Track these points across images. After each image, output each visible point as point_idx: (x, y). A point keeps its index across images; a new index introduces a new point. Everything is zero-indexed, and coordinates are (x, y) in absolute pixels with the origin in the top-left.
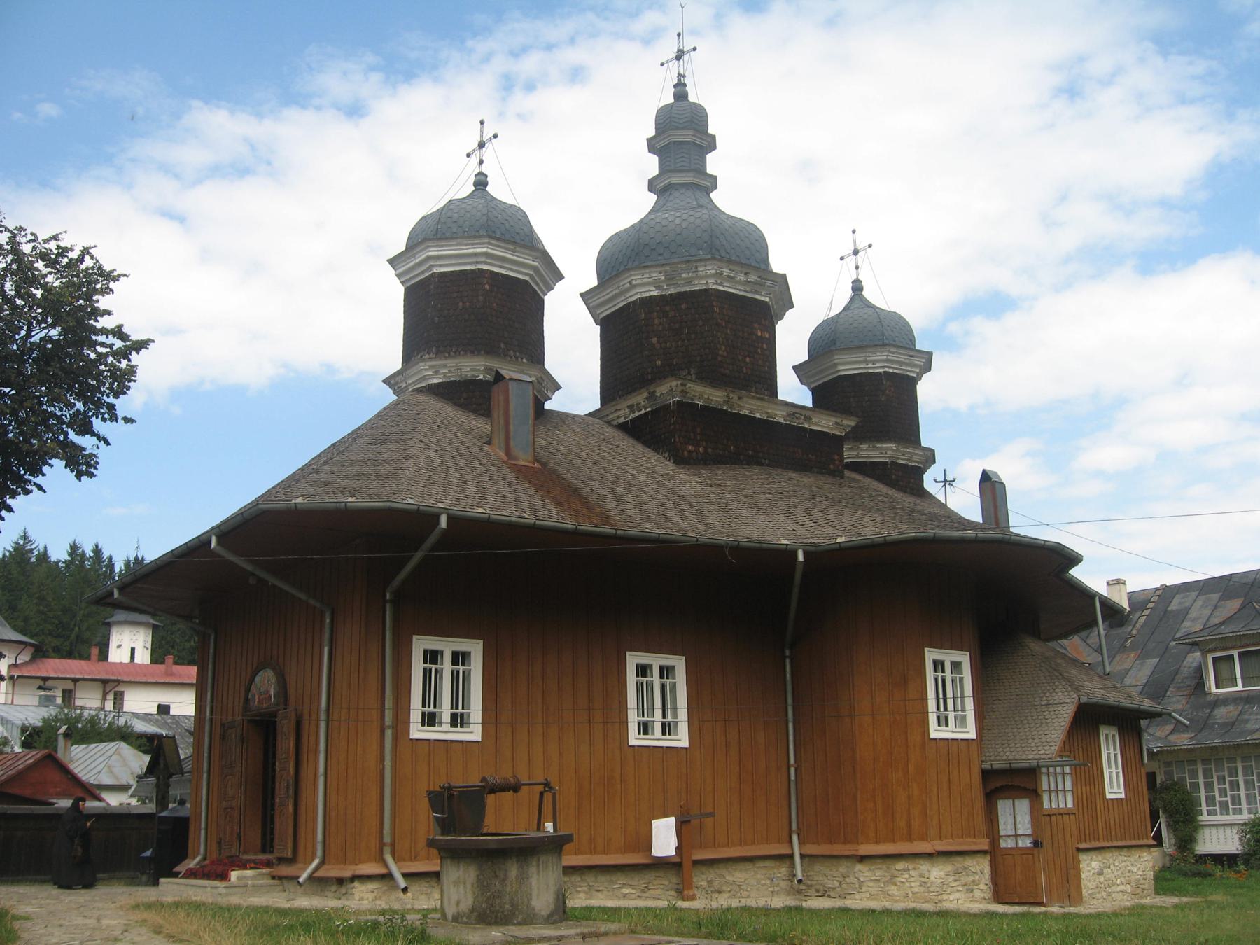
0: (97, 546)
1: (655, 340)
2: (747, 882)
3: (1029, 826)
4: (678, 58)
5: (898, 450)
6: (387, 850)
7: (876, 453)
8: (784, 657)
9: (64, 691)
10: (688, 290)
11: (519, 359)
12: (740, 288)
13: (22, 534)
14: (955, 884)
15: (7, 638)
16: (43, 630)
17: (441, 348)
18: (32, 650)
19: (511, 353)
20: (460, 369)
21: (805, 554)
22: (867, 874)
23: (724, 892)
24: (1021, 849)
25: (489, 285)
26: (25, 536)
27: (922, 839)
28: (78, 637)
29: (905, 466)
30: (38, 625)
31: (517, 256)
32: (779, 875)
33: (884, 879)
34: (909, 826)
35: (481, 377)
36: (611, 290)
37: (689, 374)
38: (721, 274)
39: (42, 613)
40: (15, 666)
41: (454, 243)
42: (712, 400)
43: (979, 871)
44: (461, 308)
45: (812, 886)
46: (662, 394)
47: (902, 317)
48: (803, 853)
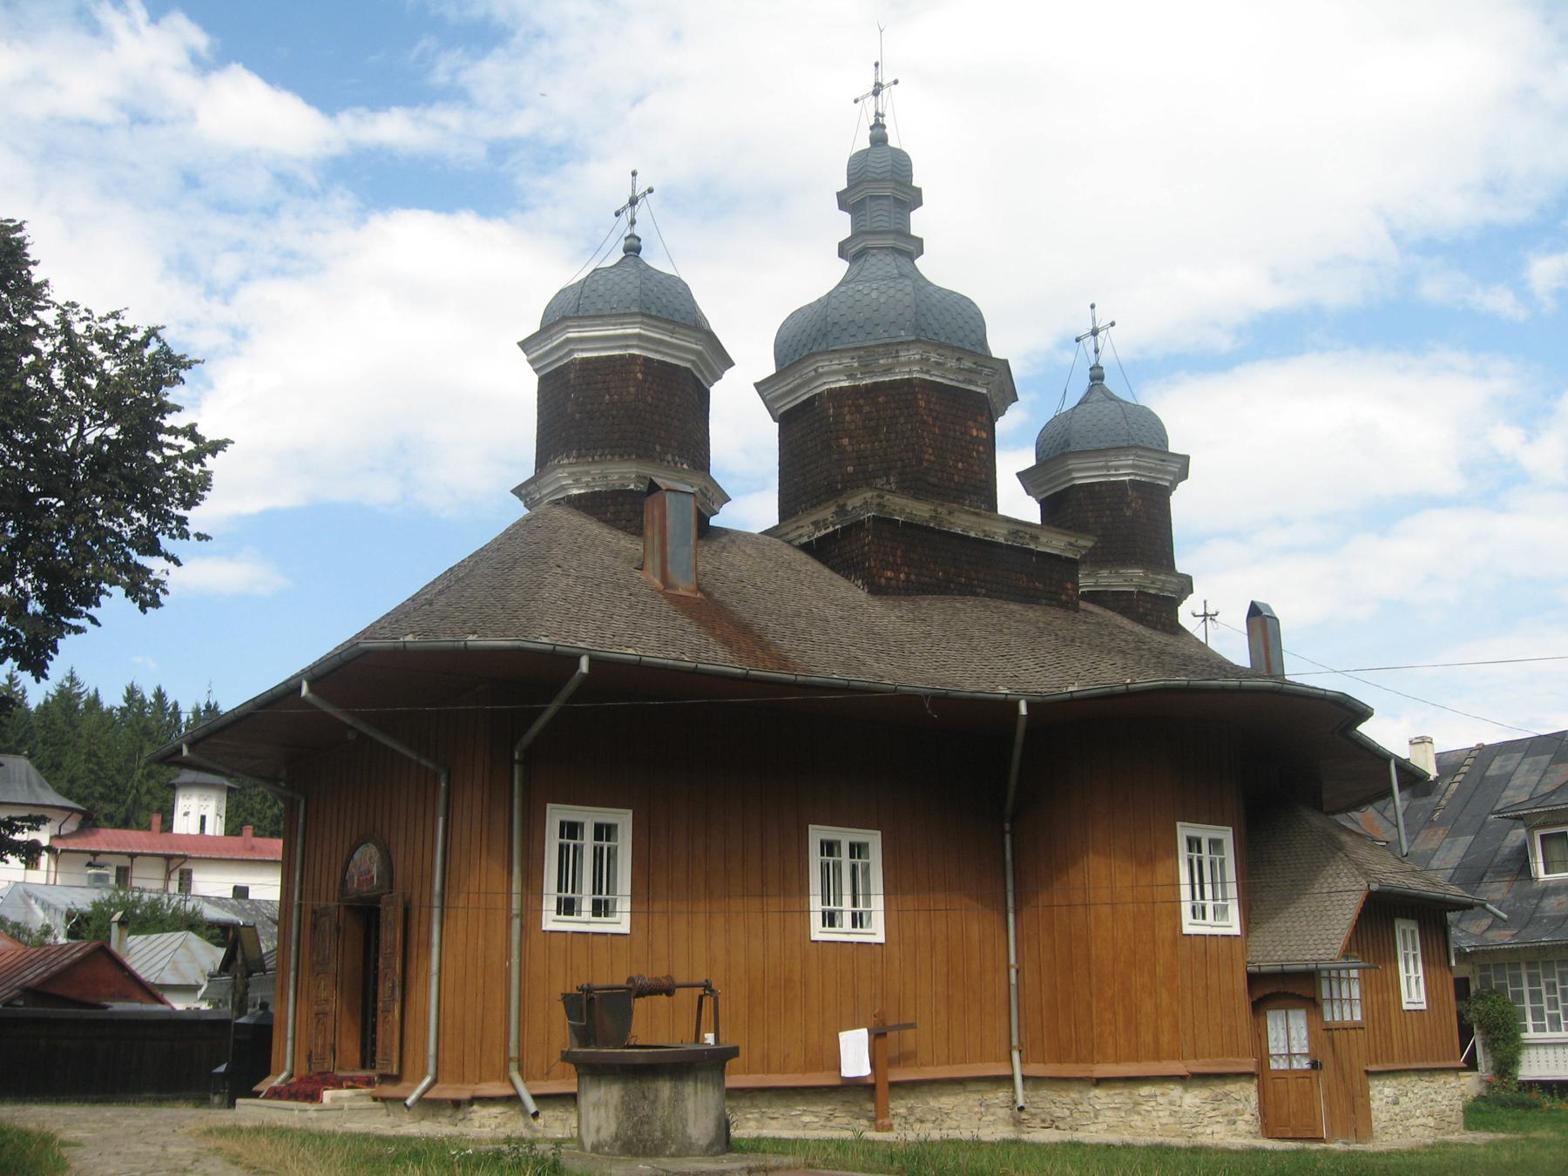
0: (159, 689)
1: (846, 441)
2: (955, 1109)
3: (1306, 1042)
4: (876, 93)
6: (513, 1067)
7: (1120, 581)
8: (1003, 833)
11: (679, 465)
12: (951, 377)
16: (93, 793)
18: (80, 817)
19: (669, 457)
24: (1296, 1071)
25: (642, 373)
27: (1173, 1058)
28: (135, 801)
29: (1156, 596)
30: (87, 787)
31: (677, 339)
32: (996, 1101)
33: (1125, 1107)
35: (632, 487)
38: (928, 360)
39: (91, 771)
41: (599, 322)
42: (916, 515)
43: (1243, 1099)
45: (1036, 1114)
46: (854, 508)
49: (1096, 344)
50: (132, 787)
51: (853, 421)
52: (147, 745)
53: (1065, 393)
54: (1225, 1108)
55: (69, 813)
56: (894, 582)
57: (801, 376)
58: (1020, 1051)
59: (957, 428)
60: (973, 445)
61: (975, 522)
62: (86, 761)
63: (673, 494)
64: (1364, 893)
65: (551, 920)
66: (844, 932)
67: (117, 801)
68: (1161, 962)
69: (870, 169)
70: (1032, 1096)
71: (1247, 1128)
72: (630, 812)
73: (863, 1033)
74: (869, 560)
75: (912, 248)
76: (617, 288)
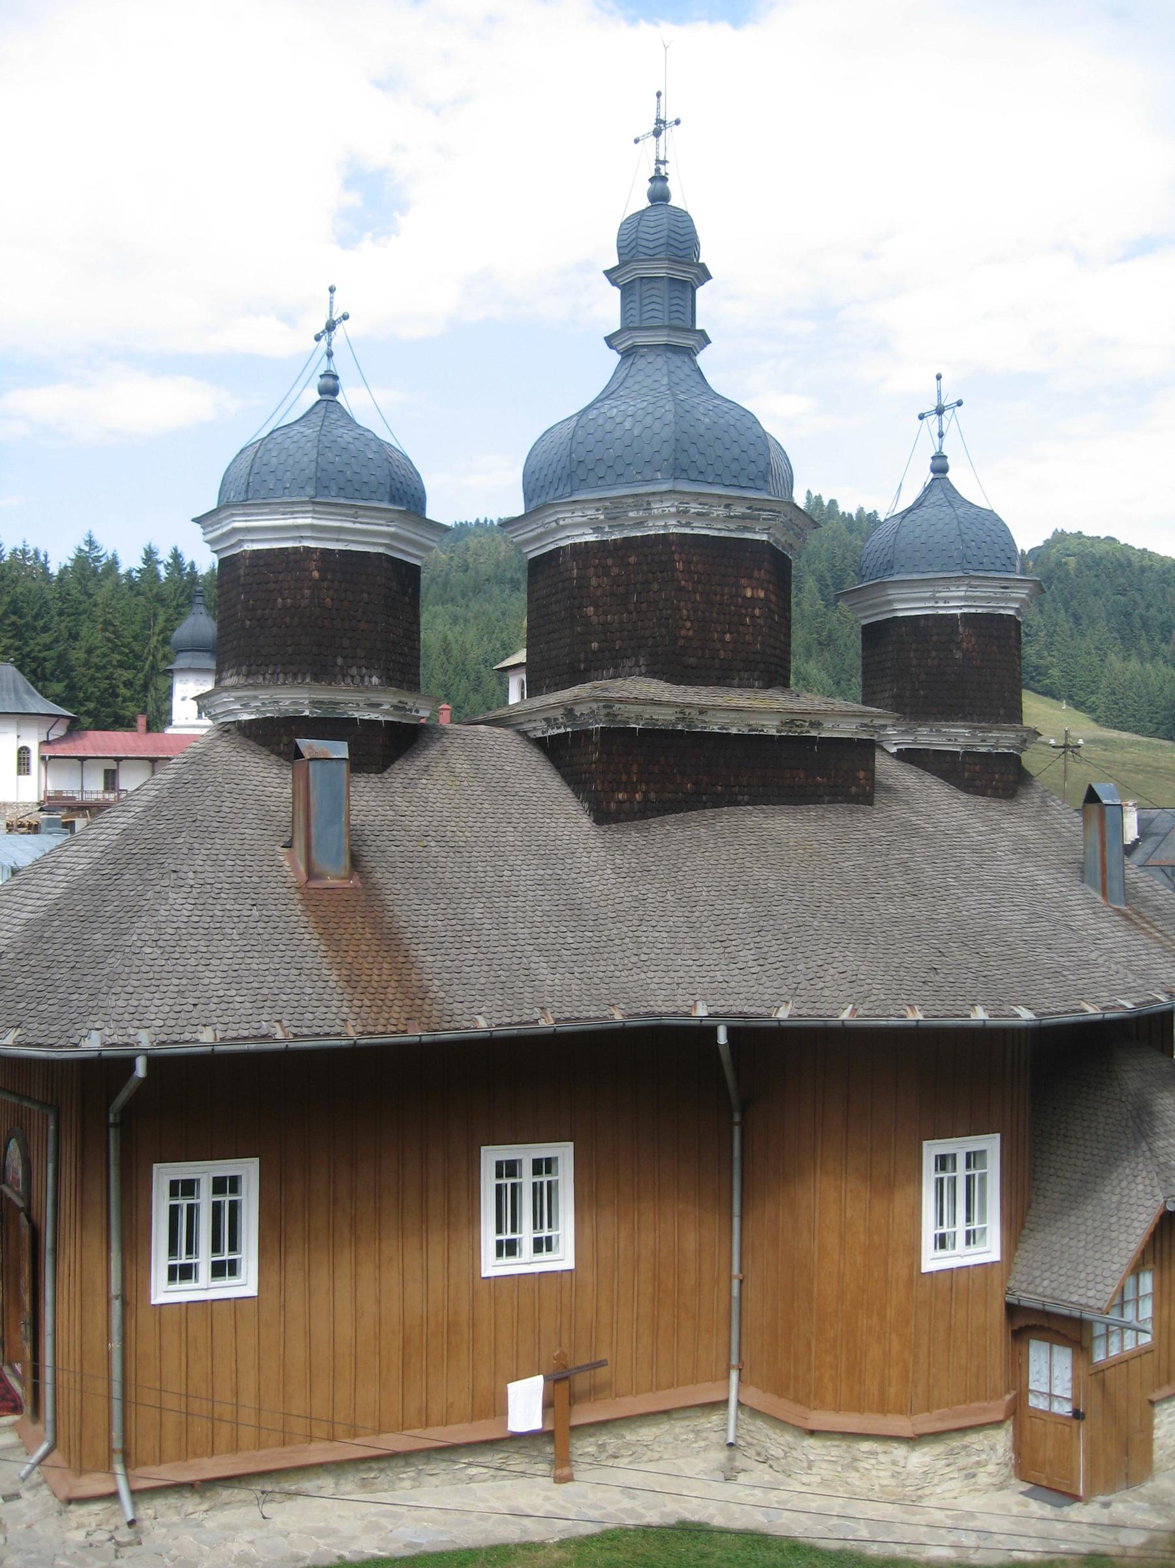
0: (176, 550)
1: (590, 610)
2: (657, 1439)
3: (1069, 1385)
4: (657, 133)
5: (974, 736)
6: (117, 1458)
7: (943, 740)
8: (731, 1124)
9: (106, 772)
10: (639, 534)
11: (367, 679)
12: (719, 527)
13: (88, 539)
14: (948, 1469)
15: (35, 711)
16: (111, 661)
17: (254, 667)
18: (67, 722)
19: (354, 671)
20: (277, 702)
21: (731, 1031)
23: (622, 1456)
25: (318, 571)
26: (90, 540)
27: (900, 1411)
28: (153, 667)
29: (988, 754)
31: (361, 523)
32: (709, 1425)
33: (842, 1461)
34: (882, 1392)
35: (307, 713)
38: (686, 512)
39: (108, 640)
40: (47, 743)
41: (266, 510)
42: (657, 720)
43: (987, 1448)
45: (752, 1444)
46: (582, 714)
47: (999, 520)
48: (742, 1400)
49: (941, 426)
50: (149, 653)
51: (599, 585)
52: (161, 610)
53: (899, 489)
54: (963, 1461)
55: (56, 719)
56: (627, 805)
57: (543, 525)
58: (740, 1370)
59: (726, 589)
61: (735, 718)
63: (318, 764)
64: (1158, 1211)
66: (527, 1262)
67: (135, 668)
69: (641, 249)
70: (749, 1424)
71: (990, 1481)
74: (596, 782)
75: (692, 343)
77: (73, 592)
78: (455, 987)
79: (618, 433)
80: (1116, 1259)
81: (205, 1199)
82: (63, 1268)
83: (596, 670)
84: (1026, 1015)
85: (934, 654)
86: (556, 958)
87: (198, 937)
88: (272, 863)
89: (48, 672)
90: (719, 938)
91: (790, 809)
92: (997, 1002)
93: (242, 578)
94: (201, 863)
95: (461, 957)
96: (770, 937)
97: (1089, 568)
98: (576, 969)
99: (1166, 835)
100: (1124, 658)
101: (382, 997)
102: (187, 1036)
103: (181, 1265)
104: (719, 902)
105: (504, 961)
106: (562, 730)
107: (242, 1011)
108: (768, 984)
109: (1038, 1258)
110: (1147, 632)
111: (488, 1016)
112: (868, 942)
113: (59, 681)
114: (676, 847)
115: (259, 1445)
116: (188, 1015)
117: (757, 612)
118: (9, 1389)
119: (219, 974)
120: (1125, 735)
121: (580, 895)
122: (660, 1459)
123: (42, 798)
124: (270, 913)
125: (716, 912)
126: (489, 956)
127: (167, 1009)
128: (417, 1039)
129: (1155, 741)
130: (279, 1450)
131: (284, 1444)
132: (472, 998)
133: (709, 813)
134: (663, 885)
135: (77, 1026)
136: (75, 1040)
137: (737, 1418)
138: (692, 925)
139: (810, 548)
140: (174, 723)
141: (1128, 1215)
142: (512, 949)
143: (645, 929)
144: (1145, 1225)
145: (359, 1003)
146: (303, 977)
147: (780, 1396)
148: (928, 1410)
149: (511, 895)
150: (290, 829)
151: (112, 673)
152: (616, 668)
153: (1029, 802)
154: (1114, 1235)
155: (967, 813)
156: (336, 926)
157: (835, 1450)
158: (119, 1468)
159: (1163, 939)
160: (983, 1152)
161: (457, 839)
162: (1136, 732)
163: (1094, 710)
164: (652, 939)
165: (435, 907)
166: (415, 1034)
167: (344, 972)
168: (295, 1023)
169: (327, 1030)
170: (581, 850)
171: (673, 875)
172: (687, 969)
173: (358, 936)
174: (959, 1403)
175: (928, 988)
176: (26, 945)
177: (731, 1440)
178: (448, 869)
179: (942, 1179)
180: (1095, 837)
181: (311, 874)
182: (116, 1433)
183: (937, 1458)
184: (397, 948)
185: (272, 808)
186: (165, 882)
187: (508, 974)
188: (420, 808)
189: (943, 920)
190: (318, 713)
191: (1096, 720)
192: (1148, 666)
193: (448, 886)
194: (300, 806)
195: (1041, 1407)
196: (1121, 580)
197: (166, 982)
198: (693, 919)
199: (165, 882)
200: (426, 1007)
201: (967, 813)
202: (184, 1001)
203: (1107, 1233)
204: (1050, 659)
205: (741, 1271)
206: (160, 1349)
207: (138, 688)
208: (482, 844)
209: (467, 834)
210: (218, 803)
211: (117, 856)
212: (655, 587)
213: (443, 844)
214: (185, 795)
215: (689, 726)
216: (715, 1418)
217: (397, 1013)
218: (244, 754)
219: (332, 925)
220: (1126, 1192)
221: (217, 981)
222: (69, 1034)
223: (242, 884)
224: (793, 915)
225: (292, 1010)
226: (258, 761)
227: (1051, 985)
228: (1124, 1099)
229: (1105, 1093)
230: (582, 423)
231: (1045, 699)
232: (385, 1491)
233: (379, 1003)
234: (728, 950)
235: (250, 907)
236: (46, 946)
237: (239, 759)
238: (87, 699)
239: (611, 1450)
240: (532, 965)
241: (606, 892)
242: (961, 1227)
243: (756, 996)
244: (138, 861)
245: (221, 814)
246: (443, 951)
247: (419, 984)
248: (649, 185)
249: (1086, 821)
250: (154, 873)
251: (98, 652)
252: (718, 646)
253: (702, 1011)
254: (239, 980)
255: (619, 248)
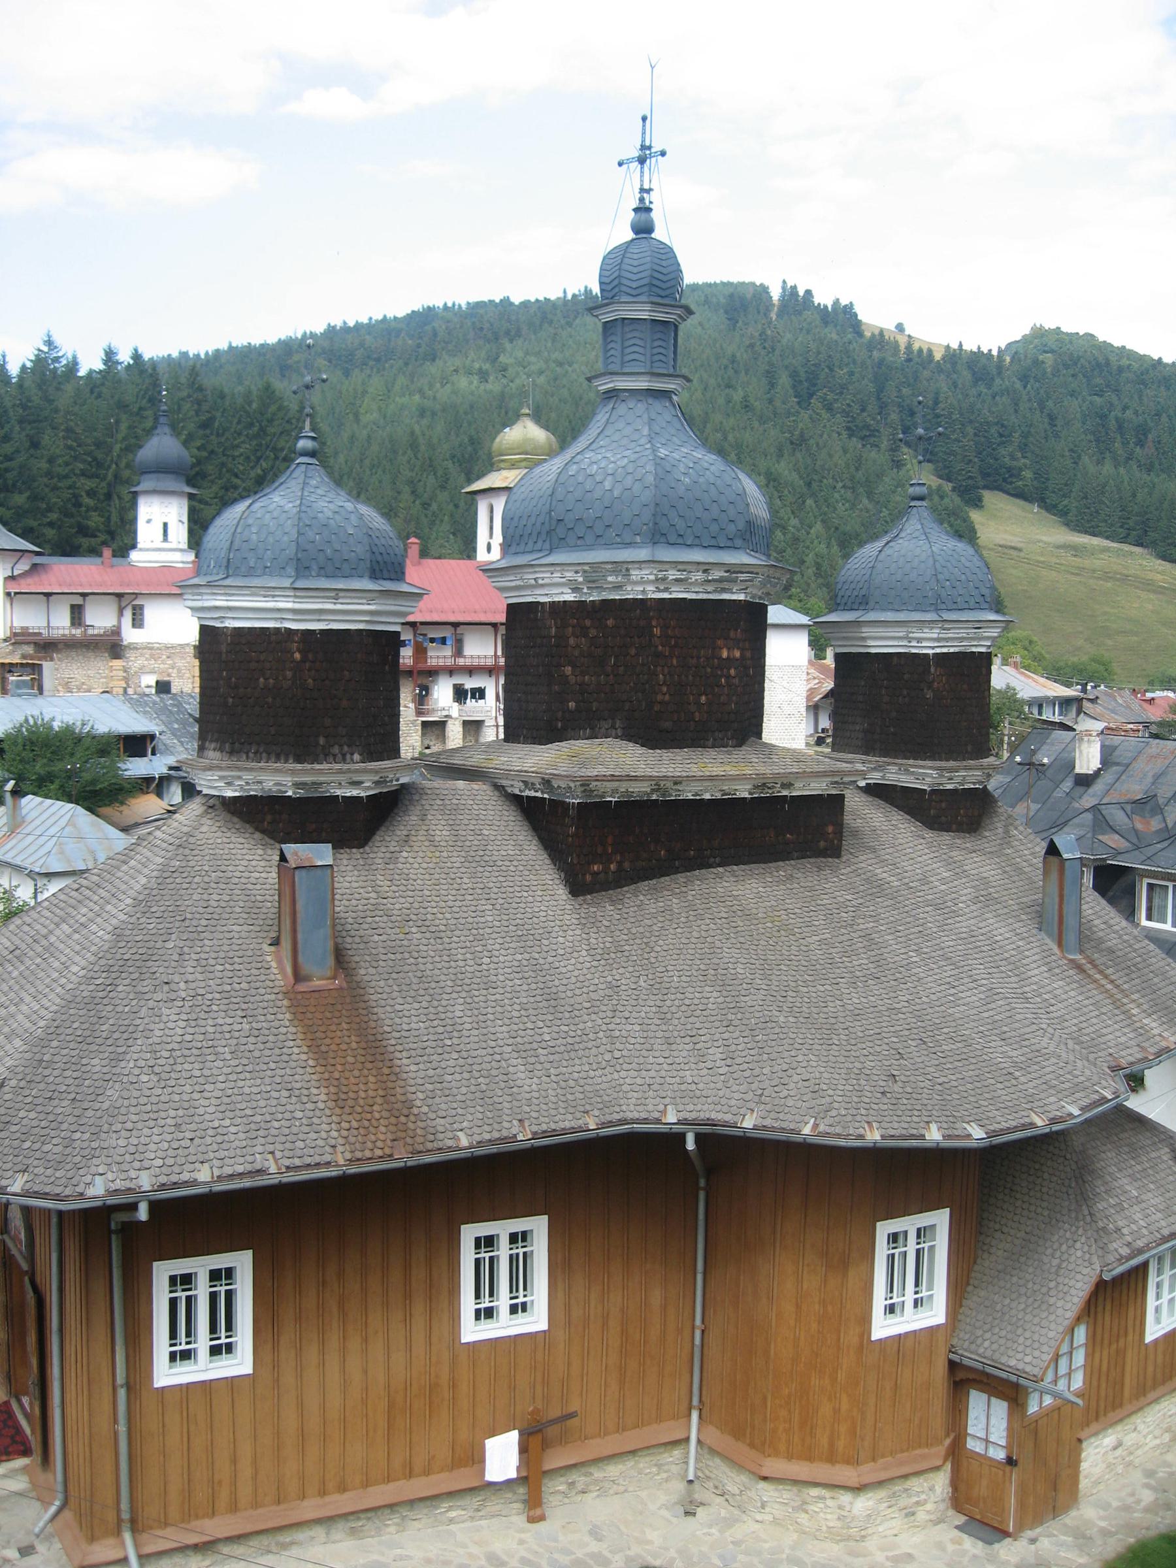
0: (136, 350)
3: (1005, 1434)
6: (126, 1527)
7: (911, 778)
8: (697, 1189)
9: (73, 607)
11: (348, 756)
14: (890, 1510)
17: (237, 745)
21: (699, 1137)
22: (772, 1493)
24: (991, 1459)
28: (116, 476)
29: (955, 791)
30: (67, 464)
34: (832, 1444)
35: (290, 793)
36: (512, 578)
37: (613, 727)
39: (70, 448)
40: (12, 578)
43: (926, 1489)
44: (261, 686)
50: (112, 461)
52: (124, 417)
54: (904, 1501)
56: (602, 876)
57: (521, 579)
60: (722, 670)
62: (64, 438)
63: (304, 872)
65: (165, 1375)
66: (505, 1326)
67: (97, 476)
68: (844, 1367)
69: (624, 288)
71: (928, 1517)
72: (250, 1253)
73: (513, 1436)
76: (271, 540)
77: (35, 398)
78: (437, 1100)
79: (598, 494)
80: (1053, 1326)
81: (202, 1291)
82: (70, 1350)
83: (573, 729)
84: (977, 1133)
85: (905, 692)
86: (533, 1060)
87: (192, 1059)
88: (259, 965)
89: (10, 482)
90: (689, 1033)
91: (757, 868)
92: (951, 1119)
93: (224, 656)
94: (192, 970)
95: (443, 1064)
96: (737, 1034)
97: (1066, 366)
98: (552, 1071)
99: (1128, 766)
100: (1098, 462)
101: (369, 1116)
102: (185, 1176)
103: (181, 1351)
104: (690, 989)
105: (484, 1066)
106: (539, 794)
107: (237, 1142)
108: (735, 1088)
109: (981, 1317)
110: (1122, 435)
111: (469, 1132)
112: (830, 1042)
113: (20, 493)
114: (649, 922)
115: (256, 1505)
116: (186, 1152)
117: (732, 672)
118: (18, 1429)
119: (213, 1101)
120: (1096, 541)
121: (557, 982)
122: (626, 1491)
123: (8, 634)
124: (259, 1026)
125: (687, 1002)
126: (470, 1061)
127: (166, 1145)
128: (402, 1164)
129: (1126, 547)
130: (274, 1508)
131: (279, 1502)
132: (454, 1113)
133: (681, 878)
134: (636, 968)
135: (81, 1172)
136: (79, 1189)
137: (697, 1451)
138: (663, 1016)
139: (784, 341)
140: (139, 546)
141: (1066, 1281)
142: (490, 1051)
143: (618, 1021)
144: (1081, 1294)
145: (346, 1125)
146: (294, 1100)
147: (737, 1439)
148: (874, 1460)
149: (489, 986)
150: (276, 922)
151: (75, 482)
152: (592, 728)
153: (992, 835)
154: (1052, 1301)
155: (932, 855)
156: (323, 1036)
157: (787, 1494)
158: (127, 1536)
159: (1115, 991)
160: (934, 1225)
161: (437, 922)
162: (1107, 538)
163: (1066, 514)
164: (624, 1033)
165: (416, 1005)
166: (402, 1158)
167: (333, 1090)
168: (287, 1153)
169: (317, 1159)
170: (557, 929)
171: (646, 956)
172: (658, 1068)
173: (344, 1047)
174: (902, 1451)
175: (886, 1101)
176: (27, 1071)
177: (691, 1477)
178: (429, 959)
179: (893, 1255)
180: (1053, 889)
181: (298, 976)
182: (125, 1505)
183: (880, 1501)
184: (382, 1058)
185: (259, 898)
186: (158, 996)
187: (487, 1080)
188: (402, 888)
189: (904, 1010)
190: (301, 792)
191: (1067, 525)
192: (1122, 470)
193: (430, 979)
194: (286, 909)
195: (977, 1450)
196: (1098, 381)
197: (163, 1114)
198: (665, 1009)
199: (158, 996)
200: (411, 1125)
201: (932, 855)
202: (181, 1135)
203: (1047, 1298)
204: (1023, 461)
205: (703, 1322)
206: (164, 1426)
207: (102, 497)
208: (461, 927)
209: (448, 916)
210: (205, 897)
211: (110, 962)
212: (633, 651)
213: (424, 929)
214: (172, 886)
215: (663, 795)
216: (677, 1453)
217: (383, 1133)
218: (228, 835)
219: (319, 1035)
220: (1065, 1256)
221: (211, 1109)
222: (74, 1181)
223: (232, 993)
224: (760, 1008)
225: (283, 1139)
226: (243, 841)
227: (1004, 1092)
228: (1068, 1156)
229: (1051, 1148)
230: (561, 480)
231: (1018, 501)
232: (372, 1537)
233: (366, 1123)
234: (698, 1047)
235: (240, 1020)
236: (46, 1072)
237: (225, 840)
238: (49, 510)
239: (580, 1486)
240: (511, 1069)
241: (581, 978)
242: (909, 1297)
243: (723, 1101)
244: (131, 969)
245: (210, 910)
246: (425, 1058)
247: (403, 1098)
248: (633, 213)
249: (1046, 873)
250: (146, 986)
251: (60, 461)
252: (693, 708)
253: (671, 1117)
254: (232, 1107)
255: (601, 269)
